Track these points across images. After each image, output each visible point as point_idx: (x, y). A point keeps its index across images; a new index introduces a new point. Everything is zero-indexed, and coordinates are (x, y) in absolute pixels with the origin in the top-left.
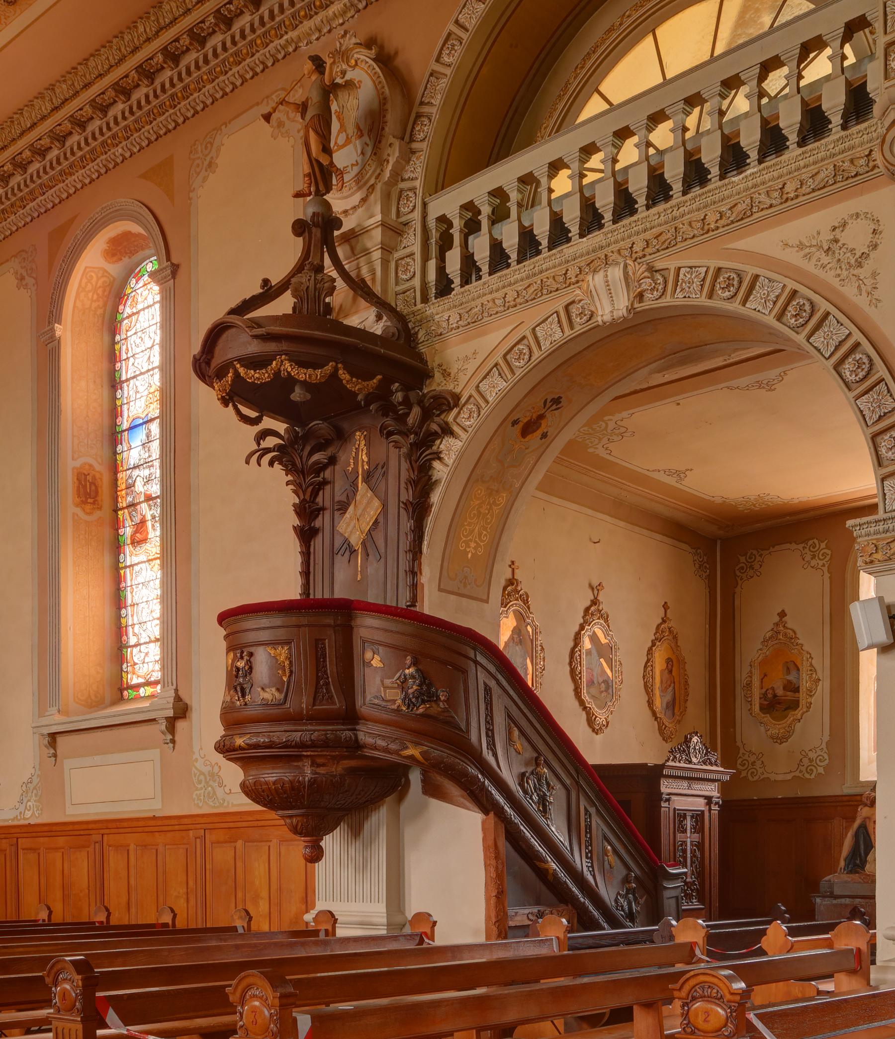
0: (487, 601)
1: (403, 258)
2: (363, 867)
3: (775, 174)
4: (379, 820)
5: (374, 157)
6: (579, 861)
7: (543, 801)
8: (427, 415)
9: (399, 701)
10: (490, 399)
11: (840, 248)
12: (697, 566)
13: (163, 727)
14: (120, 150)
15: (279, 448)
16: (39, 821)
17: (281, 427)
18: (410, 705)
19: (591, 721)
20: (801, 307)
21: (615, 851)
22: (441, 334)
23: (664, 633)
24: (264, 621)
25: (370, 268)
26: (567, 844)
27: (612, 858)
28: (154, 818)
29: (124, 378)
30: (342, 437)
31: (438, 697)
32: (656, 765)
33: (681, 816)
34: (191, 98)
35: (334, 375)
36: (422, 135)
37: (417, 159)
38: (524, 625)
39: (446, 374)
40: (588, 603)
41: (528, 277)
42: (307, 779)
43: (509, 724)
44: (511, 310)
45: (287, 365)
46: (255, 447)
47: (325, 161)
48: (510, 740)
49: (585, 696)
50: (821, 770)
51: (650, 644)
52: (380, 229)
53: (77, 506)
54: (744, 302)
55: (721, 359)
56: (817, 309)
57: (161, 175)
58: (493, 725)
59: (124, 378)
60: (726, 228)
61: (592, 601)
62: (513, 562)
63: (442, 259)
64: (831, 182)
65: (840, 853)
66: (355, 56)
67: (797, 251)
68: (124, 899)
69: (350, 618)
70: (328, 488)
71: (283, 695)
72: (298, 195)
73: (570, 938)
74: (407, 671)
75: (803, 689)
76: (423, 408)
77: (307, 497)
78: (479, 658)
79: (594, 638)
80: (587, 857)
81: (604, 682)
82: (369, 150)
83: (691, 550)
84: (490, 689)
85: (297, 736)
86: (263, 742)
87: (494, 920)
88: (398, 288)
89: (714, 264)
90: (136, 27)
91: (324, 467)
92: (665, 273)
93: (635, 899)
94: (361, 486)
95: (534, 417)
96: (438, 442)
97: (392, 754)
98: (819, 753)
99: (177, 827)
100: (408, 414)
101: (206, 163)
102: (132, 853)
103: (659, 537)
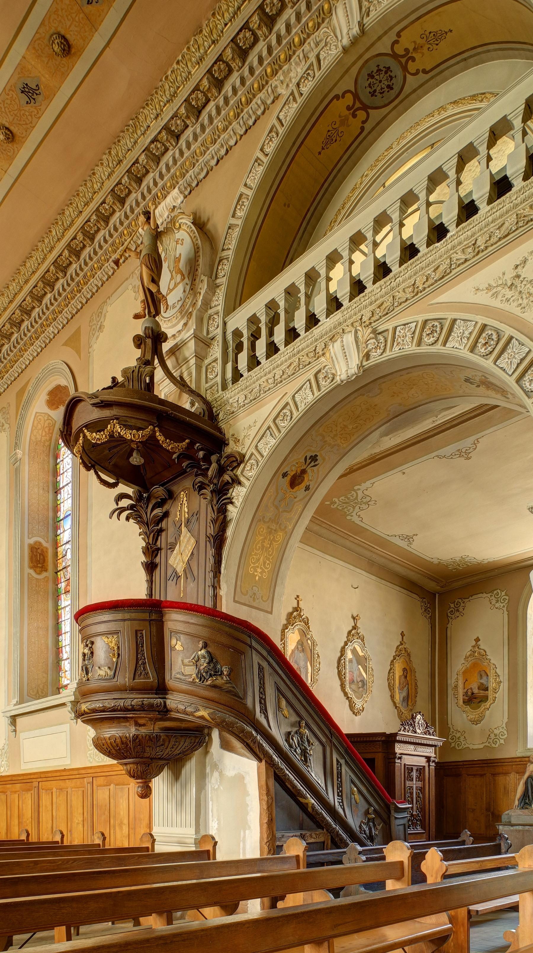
0: (271, 613)
1: (210, 364)
2: (180, 804)
3: (469, 233)
4: (190, 767)
5: (191, 292)
6: (332, 797)
7: (304, 753)
8: (221, 470)
9: (194, 675)
10: (265, 454)
11: (522, 282)
12: (423, 610)
13: (69, 709)
14: (51, 329)
15: (131, 507)
16: (8, 774)
17: (130, 491)
18: (201, 678)
19: (352, 707)
20: (490, 337)
21: (360, 792)
22: (233, 412)
23: (402, 652)
24: (106, 616)
25: (189, 373)
26: (323, 785)
27: (357, 797)
28: (65, 770)
29: (61, 486)
30: (171, 496)
31: (222, 672)
32: (391, 734)
33: (409, 769)
34: (89, 283)
35: (152, 437)
36: (223, 273)
37: (220, 290)
38: (305, 639)
39: (237, 441)
40: (351, 628)
41: (290, 358)
42: (131, 735)
43: (278, 696)
44: (279, 385)
45: (118, 428)
46: (116, 507)
47: (154, 290)
48: (279, 707)
49: (348, 690)
50: (502, 741)
51: (392, 658)
52: (193, 341)
53: (31, 568)
54: (445, 344)
55: (431, 420)
56: (503, 334)
57: (74, 342)
58: (265, 695)
59: (61, 486)
60: (431, 287)
61: (353, 627)
62: (298, 596)
63: (236, 361)
64: (514, 229)
65: (515, 795)
66: (180, 221)
67: (487, 293)
68: (50, 826)
69: (161, 615)
70: (164, 534)
71: (113, 672)
72: (137, 317)
73: (308, 856)
74: (200, 653)
75: (490, 689)
76: (219, 465)
77: (151, 542)
78: (254, 644)
79: (354, 651)
80: (338, 796)
81: (361, 681)
82: (188, 288)
83: (419, 599)
84: (263, 668)
85: (121, 703)
86: (99, 707)
87: (265, 841)
88: (207, 385)
89: (421, 318)
90: (50, 231)
91: (161, 520)
92: (385, 334)
93: (375, 826)
94: (184, 529)
95: (299, 472)
96: (231, 490)
97: (189, 715)
98: (501, 730)
99: (77, 776)
100: (208, 469)
101: (98, 326)
102: (54, 794)
103: (398, 588)
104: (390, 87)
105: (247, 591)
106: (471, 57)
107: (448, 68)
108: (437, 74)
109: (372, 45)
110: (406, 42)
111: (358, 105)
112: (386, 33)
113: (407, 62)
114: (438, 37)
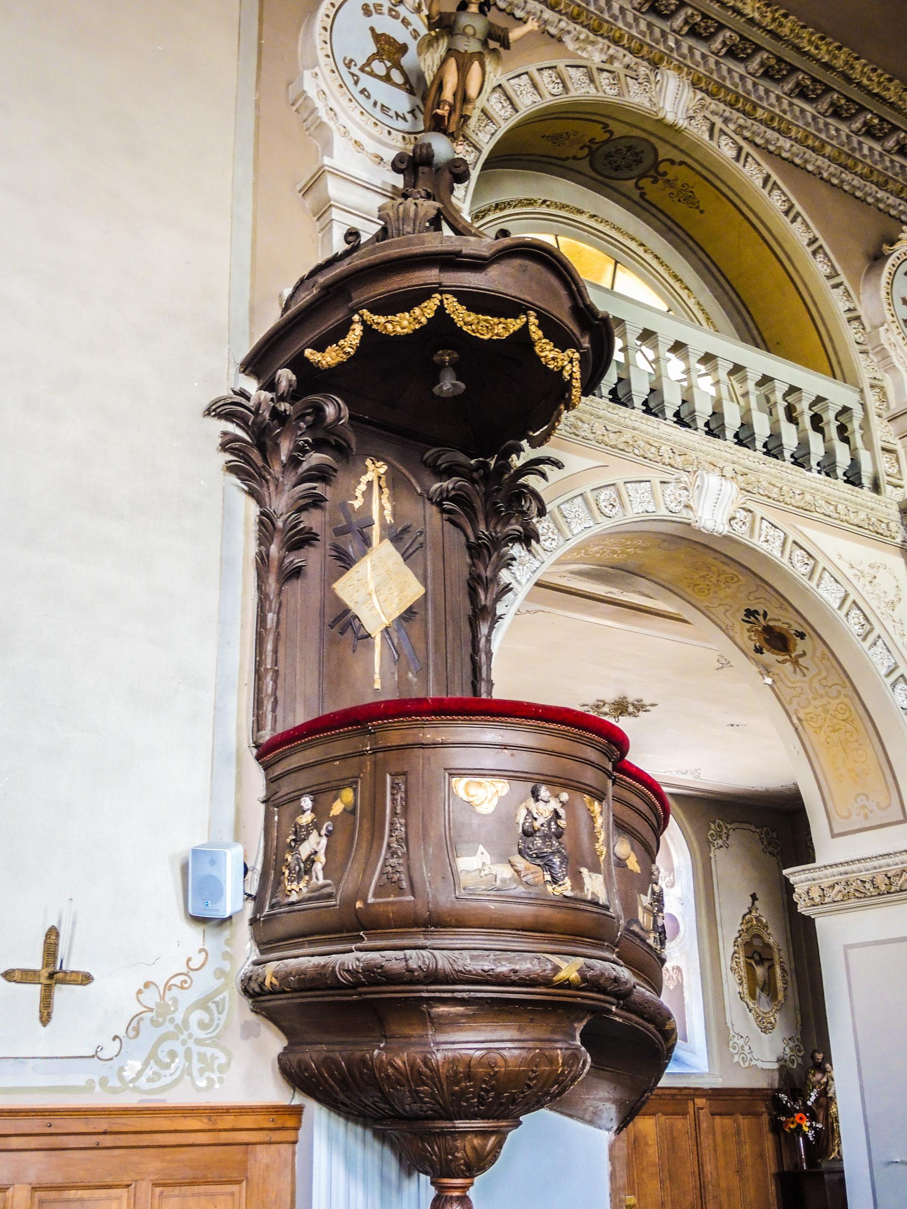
104: (617, 168)
105: (849, 811)
107: (654, 215)
108: (642, 206)
109: (666, 142)
110: (673, 172)
111: (594, 147)
112: (682, 151)
113: (651, 176)
114: (690, 199)
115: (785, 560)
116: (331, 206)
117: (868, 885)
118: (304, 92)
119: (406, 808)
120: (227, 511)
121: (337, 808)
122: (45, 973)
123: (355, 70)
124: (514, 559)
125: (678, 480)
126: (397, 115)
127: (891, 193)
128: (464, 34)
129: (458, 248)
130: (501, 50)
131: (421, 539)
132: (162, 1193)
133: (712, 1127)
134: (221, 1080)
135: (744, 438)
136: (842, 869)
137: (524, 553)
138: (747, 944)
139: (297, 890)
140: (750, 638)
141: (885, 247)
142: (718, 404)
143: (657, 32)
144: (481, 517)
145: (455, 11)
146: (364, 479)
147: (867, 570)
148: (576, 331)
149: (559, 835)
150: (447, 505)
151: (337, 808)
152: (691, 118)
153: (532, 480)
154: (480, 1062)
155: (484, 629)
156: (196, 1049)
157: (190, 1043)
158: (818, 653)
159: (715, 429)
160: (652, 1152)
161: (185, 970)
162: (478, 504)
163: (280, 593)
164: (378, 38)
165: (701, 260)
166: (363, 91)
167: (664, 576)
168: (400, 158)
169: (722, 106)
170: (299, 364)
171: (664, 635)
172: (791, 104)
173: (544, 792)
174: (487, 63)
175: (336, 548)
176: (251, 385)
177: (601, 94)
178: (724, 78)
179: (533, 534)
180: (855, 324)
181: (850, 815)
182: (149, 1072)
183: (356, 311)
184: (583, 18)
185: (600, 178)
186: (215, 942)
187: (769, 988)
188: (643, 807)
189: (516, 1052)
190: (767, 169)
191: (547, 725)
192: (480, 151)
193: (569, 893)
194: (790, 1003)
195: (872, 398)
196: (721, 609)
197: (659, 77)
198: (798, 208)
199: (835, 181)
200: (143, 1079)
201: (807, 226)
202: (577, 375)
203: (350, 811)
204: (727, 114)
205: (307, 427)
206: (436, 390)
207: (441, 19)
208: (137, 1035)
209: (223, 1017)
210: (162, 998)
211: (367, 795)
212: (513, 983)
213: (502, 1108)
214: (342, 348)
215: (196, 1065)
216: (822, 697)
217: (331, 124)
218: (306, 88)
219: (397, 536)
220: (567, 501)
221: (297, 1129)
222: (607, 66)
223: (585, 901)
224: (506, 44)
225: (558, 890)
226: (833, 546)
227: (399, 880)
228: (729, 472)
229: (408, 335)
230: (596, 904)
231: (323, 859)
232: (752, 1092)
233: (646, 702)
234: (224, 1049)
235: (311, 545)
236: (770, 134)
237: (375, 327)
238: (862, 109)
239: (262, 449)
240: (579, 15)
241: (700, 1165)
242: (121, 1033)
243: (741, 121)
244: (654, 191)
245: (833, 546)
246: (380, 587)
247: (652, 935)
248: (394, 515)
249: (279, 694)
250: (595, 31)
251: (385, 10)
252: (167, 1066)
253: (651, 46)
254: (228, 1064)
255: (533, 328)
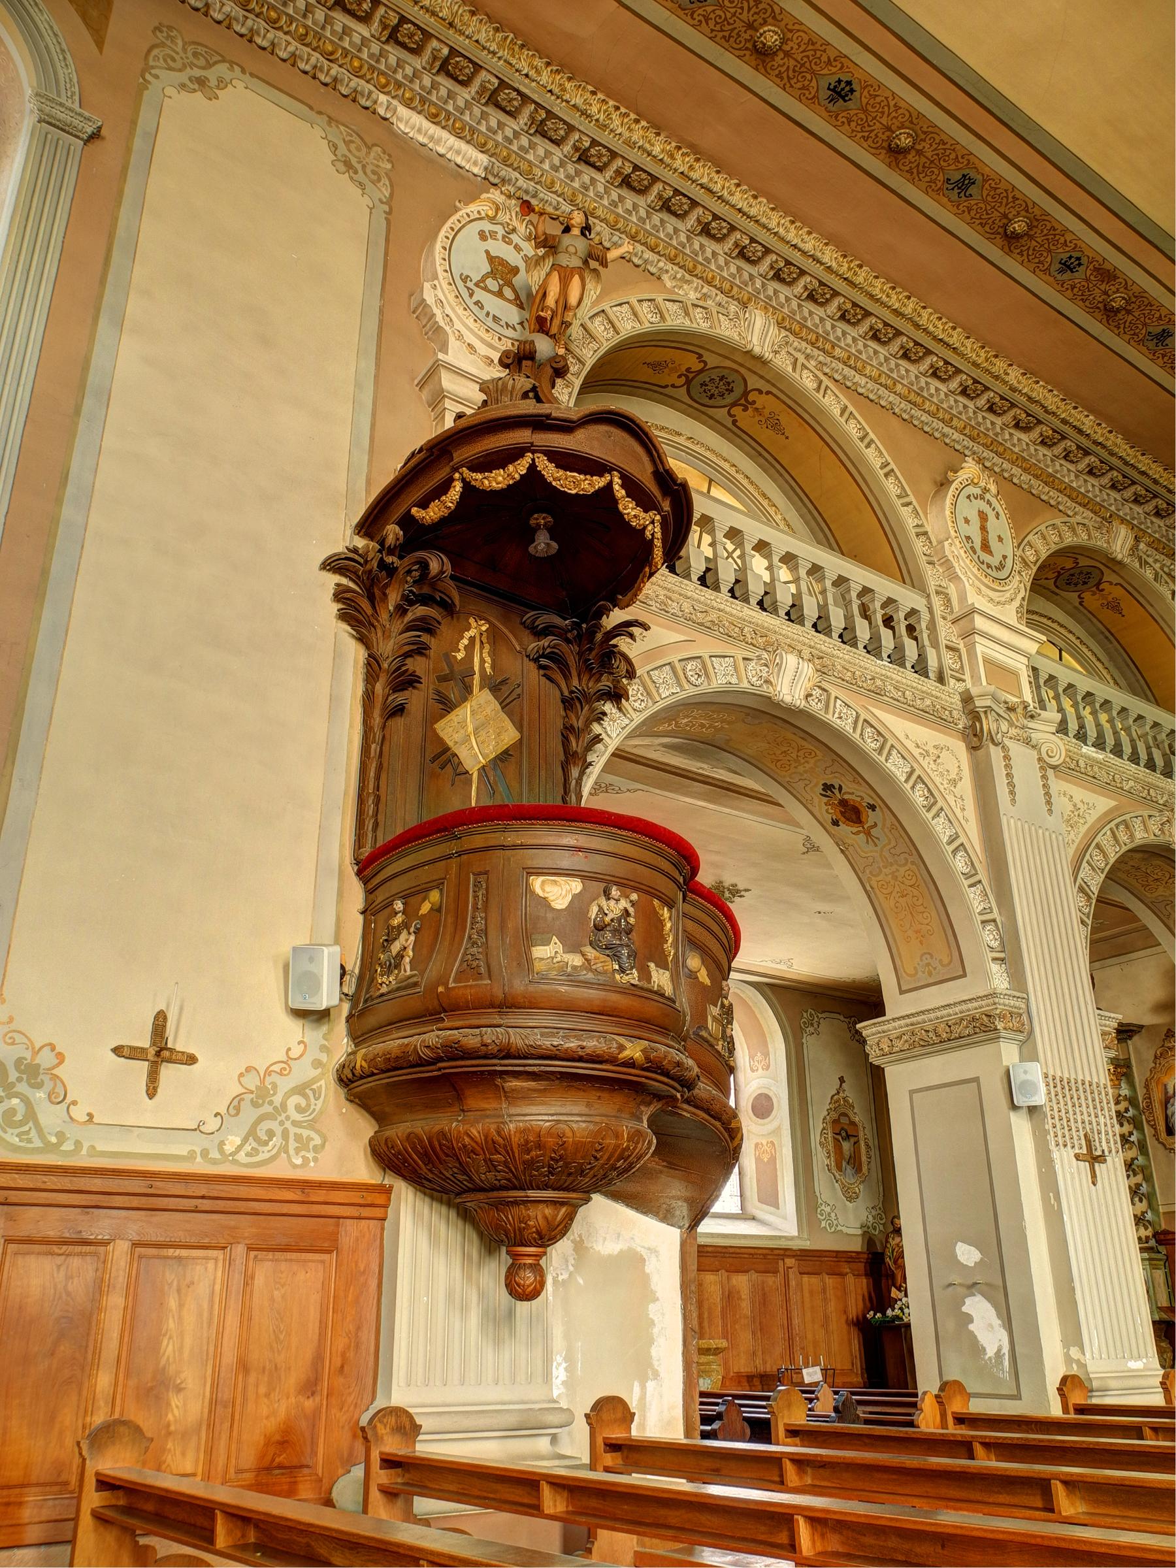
104: (711, 397)
106: (766, 460)
108: (735, 433)
109: (755, 373)
110: (761, 401)
111: (691, 376)
112: (768, 381)
114: (776, 427)
115: (857, 736)
116: (445, 396)
117: (931, 1034)
118: (424, 300)
119: (486, 902)
120: (337, 655)
121: (425, 908)
122: (152, 1051)
123: (469, 284)
124: (604, 714)
125: (759, 658)
126: (507, 325)
127: (956, 429)
128: (567, 251)
129: (548, 411)
130: (600, 268)
131: (518, 691)
132: (256, 1257)
133: (800, 1285)
134: (315, 1160)
135: (821, 625)
136: (908, 1021)
137: (614, 711)
138: (835, 1122)
139: (386, 982)
140: (827, 811)
141: (950, 474)
142: (797, 597)
143: (746, 276)
144: (574, 673)
145: (559, 233)
146: (467, 635)
147: (932, 750)
148: (660, 499)
149: (628, 932)
150: (543, 661)
151: (425, 908)
152: (776, 352)
153: (623, 643)
154: (549, 1132)
155: (575, 772)
156: (293, 1130)
157: (288, 1124)
158: (888, 824)
159: (794, 614)
160: (745, 1306)
161: (285, 1059)
162: (572, 661)
163: (384, 727)
164: (491, 259)
165: (787, 482)
166: (477, 303)
167: (749, 751)
168: (506, 354)
169: (804, 344)
170: (407, 521)
171: (755, 818)
172: (865, 346)
173: (615, 892)
174: (587, 281)
175: (438, 693)
176: (360, 543)
177: (695, 325)
178: (805, 319)
179: (622, 692)
180: (923, 538)
181: (916, 973)
182: (248, 1148)
183: (456, 470)
184: (679, 259)
185: (696, 405)
186: (314, 1035)
187: (854, 1162)
188: (715, 928)
189: (584, 1125)
190: (845, 401)
191: (619, 832)
192: (584, 365)
193: (635, 982)
194: (874, 1174)
195: (937, 602)
196: (802, 784)
197: (747, 315)
198: (872, 435)
199: (905, 416)
200: (242, 1153)
201: (880, 451)
202: (659, 535)
203: (436, 910)
204: (808, 351)
205: (414, 582)
206: (531, 549)
207: (546, 239)
208: (237, 1114)
209: (320, 1103)
210: (263, 1081)
211: (452, 894)
212: (580, 1059)
213: (571, 1178)
214: (444, 503)
215: (292, 1145)
216: (891, 864)
217: (447, 328)
218: (425, 297)
219: (496, 686)
220: (656, 669)
221: (386, 1206)
222: (701, 303)
223: (651, 991)
224: (604, 263)
225: (626, 979)
226: (899, 726)
227: (478, 966)
228: (806, 655)
229: (502, 489)
230: (663, 995)
231: (411, 953)
232: (838, 1255)
233: (741, 887)
234: (317, 1132)
235: (414, 688)
236: (847, 370)
237: (473, 483)
238: (928, 352)
239: (371, 599)
240: (676, 256)
241: (789, 1319)
242: (223, 1111)
243: (821, 358)
244: (745, 418)
245: (899, 726)
246: (477, 732)
247: (720, 1043)
248: (493, 667)
249: (381, 817)
250: (690, 272)
251: (499, 236)
252: (266, 1143)
253: (740, 288)
254: (323, 1145)
255: (616, 487)
